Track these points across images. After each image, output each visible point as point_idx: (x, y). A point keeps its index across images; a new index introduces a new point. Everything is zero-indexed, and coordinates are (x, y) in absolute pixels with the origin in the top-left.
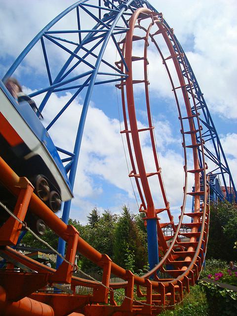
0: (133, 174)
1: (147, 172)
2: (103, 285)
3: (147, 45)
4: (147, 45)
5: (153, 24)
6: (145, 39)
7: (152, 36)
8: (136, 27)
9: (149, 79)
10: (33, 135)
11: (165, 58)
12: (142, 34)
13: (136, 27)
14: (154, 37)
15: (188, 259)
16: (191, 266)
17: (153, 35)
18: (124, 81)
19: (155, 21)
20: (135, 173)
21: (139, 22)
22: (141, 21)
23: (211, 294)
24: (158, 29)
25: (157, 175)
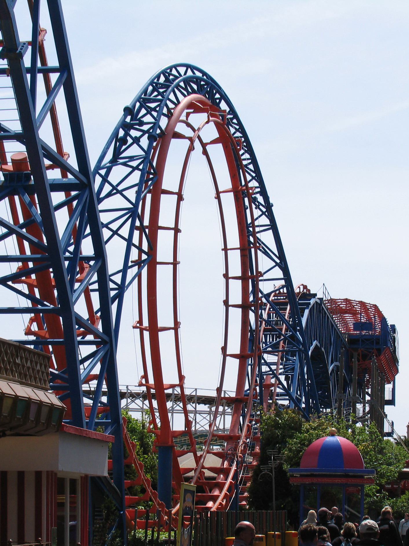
0: (138, 325)
1: (160, 324)
2: (28, 207)
3: (191, 148)
4: (191, 148)
5: (207, 122)
6: (191, 139)
7: (204, 145)
8: (183, 121)
9: (184, 193)
10: (66, 227)
11: (220, 190)
12: (188, 132)
13: (183, 121)
14: (208, 148)
15: (216, 493)
16: (219, 501)
17: (207, 144)
18: (151, 176)
19: (211, 118)
20: (147, 381)
21: (188, 115)
22: (191, 115)
23: (373, 436)
24: (216, 135)
25: (172, 266)
